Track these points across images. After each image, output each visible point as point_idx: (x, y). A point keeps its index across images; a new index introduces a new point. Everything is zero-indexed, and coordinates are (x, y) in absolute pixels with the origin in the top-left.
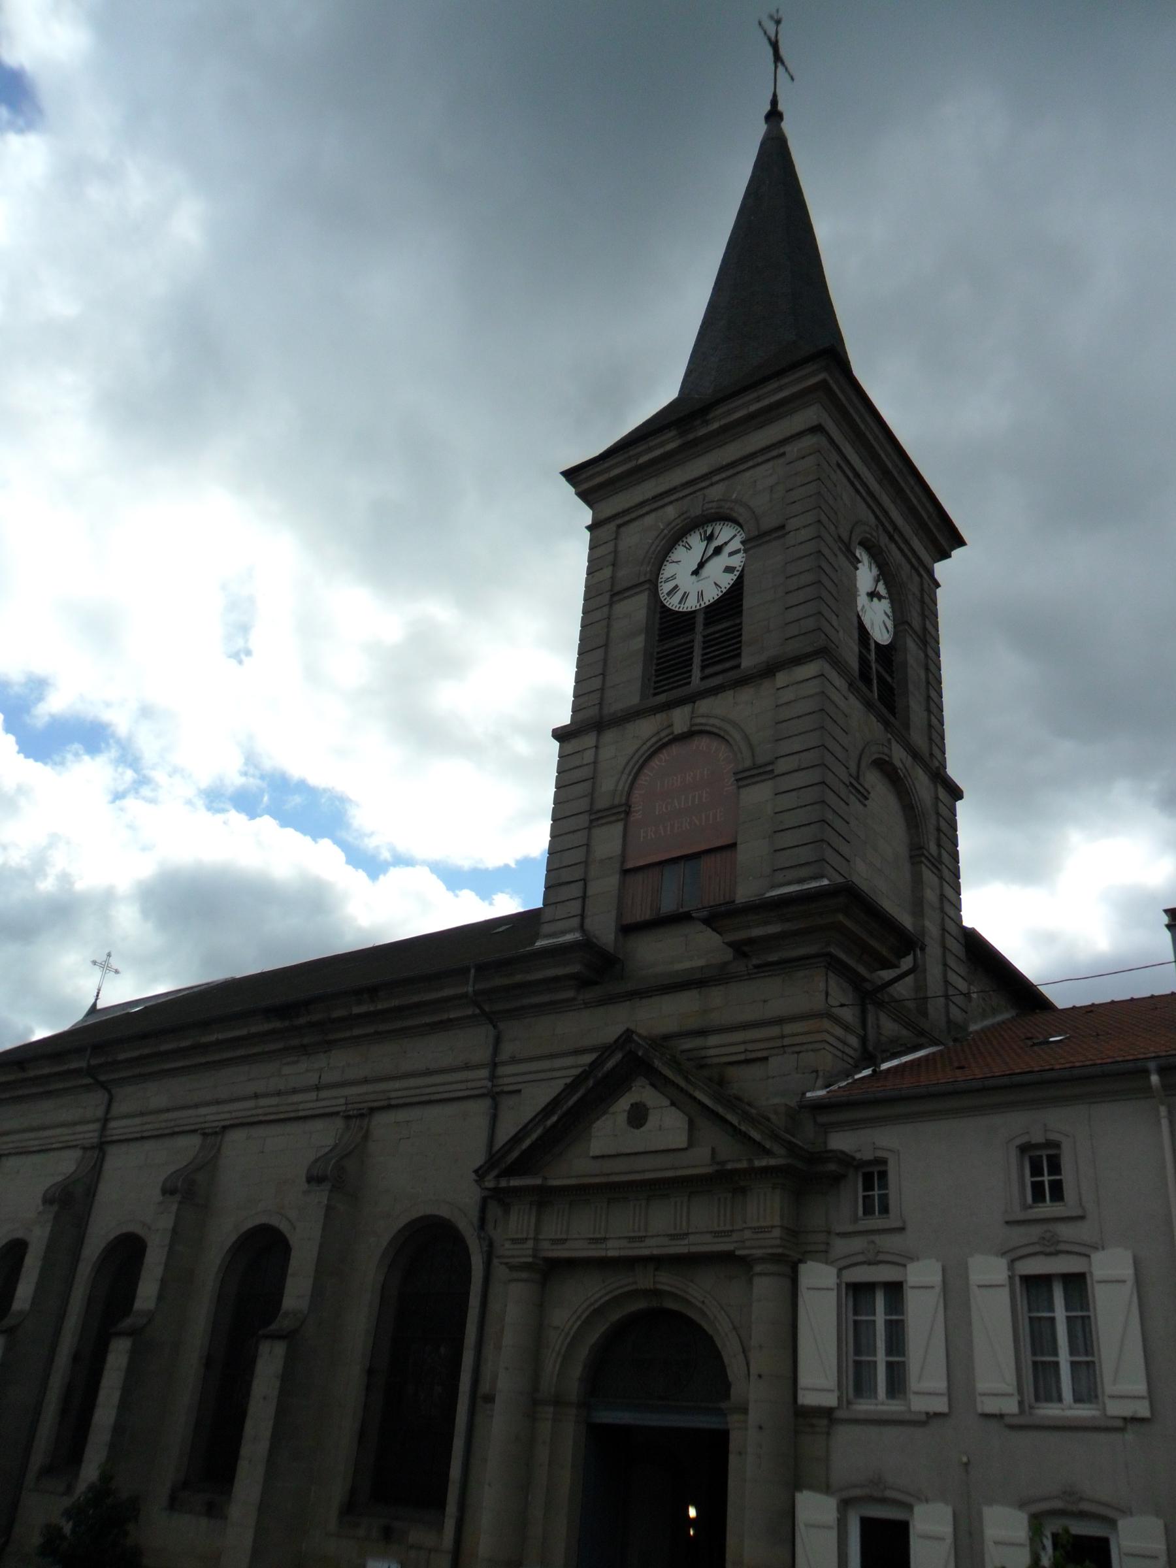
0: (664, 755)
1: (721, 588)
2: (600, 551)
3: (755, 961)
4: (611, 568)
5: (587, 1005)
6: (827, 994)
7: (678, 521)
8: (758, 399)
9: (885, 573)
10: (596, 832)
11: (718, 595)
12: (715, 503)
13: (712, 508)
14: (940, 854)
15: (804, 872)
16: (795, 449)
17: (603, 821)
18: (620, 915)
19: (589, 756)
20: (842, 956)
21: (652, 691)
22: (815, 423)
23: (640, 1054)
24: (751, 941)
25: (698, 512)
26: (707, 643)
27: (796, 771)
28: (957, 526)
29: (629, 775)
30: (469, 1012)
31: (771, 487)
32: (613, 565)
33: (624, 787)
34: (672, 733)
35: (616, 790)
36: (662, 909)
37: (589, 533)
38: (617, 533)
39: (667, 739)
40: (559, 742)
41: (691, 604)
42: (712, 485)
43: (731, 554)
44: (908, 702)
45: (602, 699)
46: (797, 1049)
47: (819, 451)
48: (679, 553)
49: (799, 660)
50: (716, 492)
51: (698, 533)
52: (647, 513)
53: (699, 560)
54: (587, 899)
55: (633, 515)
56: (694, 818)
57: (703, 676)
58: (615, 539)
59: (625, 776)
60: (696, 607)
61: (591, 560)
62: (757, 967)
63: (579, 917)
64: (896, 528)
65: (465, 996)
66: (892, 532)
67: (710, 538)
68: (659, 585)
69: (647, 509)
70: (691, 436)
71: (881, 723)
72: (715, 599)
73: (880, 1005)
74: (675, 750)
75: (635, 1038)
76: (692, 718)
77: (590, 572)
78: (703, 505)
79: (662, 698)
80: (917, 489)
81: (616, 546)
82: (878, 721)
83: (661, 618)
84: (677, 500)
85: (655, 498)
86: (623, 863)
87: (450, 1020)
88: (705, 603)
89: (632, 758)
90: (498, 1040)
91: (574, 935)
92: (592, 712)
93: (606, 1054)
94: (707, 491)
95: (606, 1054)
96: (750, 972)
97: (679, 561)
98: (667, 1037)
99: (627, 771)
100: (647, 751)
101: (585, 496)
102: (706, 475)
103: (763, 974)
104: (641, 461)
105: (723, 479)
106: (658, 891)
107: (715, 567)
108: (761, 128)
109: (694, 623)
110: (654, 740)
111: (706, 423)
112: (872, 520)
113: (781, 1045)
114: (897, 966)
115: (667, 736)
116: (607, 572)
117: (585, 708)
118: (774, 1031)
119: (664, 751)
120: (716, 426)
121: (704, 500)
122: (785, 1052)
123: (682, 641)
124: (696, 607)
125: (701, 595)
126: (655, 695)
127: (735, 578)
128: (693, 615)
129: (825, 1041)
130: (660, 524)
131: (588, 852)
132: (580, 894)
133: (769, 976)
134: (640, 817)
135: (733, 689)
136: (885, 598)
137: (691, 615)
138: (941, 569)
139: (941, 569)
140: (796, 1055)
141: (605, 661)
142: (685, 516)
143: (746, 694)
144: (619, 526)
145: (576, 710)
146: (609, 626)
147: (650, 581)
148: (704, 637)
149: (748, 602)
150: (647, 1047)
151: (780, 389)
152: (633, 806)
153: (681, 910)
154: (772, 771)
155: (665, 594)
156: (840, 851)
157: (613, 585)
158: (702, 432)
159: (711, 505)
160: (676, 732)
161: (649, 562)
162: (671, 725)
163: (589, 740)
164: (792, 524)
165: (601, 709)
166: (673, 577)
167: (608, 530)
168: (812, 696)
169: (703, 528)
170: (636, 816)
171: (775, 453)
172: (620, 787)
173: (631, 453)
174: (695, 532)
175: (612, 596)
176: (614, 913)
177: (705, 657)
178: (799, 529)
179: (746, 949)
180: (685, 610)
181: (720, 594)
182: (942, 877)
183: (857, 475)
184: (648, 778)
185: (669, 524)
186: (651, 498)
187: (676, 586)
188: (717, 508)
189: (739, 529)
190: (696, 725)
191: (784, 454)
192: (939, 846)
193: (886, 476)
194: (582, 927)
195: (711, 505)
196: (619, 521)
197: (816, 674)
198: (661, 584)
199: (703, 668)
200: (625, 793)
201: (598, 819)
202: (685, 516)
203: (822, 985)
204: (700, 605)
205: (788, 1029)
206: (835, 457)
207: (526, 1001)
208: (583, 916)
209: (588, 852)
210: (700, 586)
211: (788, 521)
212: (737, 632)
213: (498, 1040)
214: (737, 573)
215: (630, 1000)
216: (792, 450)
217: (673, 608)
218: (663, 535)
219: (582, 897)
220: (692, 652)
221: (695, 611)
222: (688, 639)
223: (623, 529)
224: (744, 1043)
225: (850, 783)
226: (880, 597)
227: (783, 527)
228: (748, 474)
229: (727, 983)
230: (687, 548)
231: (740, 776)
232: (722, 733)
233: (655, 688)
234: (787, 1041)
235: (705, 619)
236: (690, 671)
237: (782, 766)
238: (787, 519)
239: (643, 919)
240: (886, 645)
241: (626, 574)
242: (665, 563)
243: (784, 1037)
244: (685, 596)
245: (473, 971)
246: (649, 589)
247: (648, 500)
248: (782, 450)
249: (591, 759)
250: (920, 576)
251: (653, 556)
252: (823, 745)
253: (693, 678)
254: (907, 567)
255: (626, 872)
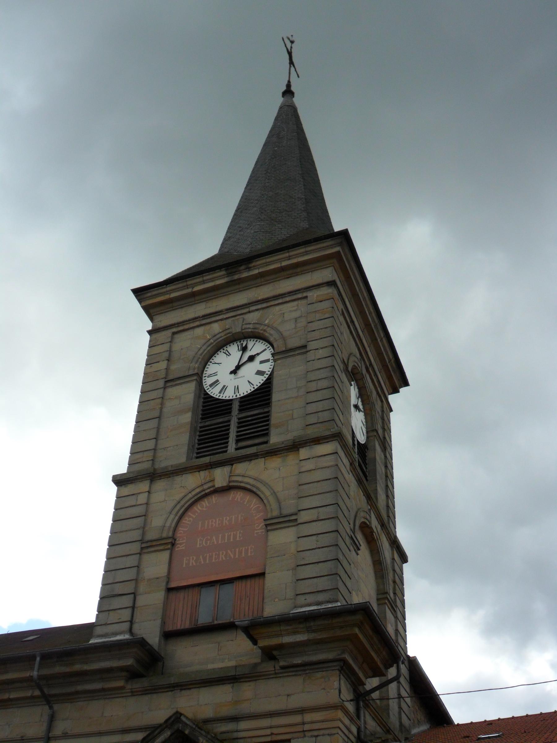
0: (205, 503)
1: (253, 385)
2: (157, 350)
3: (282, 663)
4: (166, 362)
5: (134, 693)
6: (340, 692)
7: (222, 334)
8: (289, 258)
9: (363, 394)
10: (146, 558)
11: (251, 390)
12: (251, 325)
13: (249, 328)
14: (395, 599)
15: (321, 597)
16: (315, 295)
17: (153, 549)
18: (163, 623)
19: (142, 499)
20: (351, 661)
21: (195, 455)
22: (331, 279)
23: (187, 732)
24: (281, 647)
25: (238, 330)
26: (241, 423)
27: (316, 521)
28: (405, 371)
29: (176, 515)
30: (29, 694)
31: (296, 318)
32: (168, 360)
33: (171, 524)
34: (214, 486)
35: (164, 526)
36: (199, 621)
37: (149, 336)
38: (172, 338)
39: (209, 490)
40: (117, 486)
41: (229, 395)
42: (249, 312)
43: (261, 362)
44: (377, 486)
45: (154, 456)
46: (315, 733)
47: (333, 298)
48: (220, 357)
49: (318, 441)
50: (253, 317)
51: (236, 345)
52: (198, 326)
53: (237, 364)
54: (135, 609)
55: (186, 327)
56: (229, 551)
57: (238, 447)
58: (170, 342)
59: (172, 516)
60: (233, 397)
61: (150, 355)
62: (283, 668)
63: (128, 623)
64: (371, 364)
65: (30, 679)
66: (368, 366)
67: (244, 349)
68: (204, 378)
69: (197, 323)
70: (236, 277)
71: (365, 497)
72: (249, 392)
73: (367, 706)
74: (214, 499)
75: (183, 718)
76: (230, 476)
77: (149, 363)
78: (243, 325)
79: (207, 460)
80: (384, 340)
81: (171, 347)
82: (364, 495)
83: (204, 403)
84: (221, 320)
85: (205, 316)
86: (168, 582)
87: (10, 700)
88: (240, 395)
89: (179, 502)
90: (52, 718)
91: (124, 636)
92: (146, 466)
93: (157, 732)
94: (246, 316)
95: (157, 732)
96: (276, 671)
97: (221, 363)
98: (207, 721)
99: (174, 512)
100: (191, 498)
101: (148, 310)
102: (246, 305)
103: (286, 674)
104: (197, 289)
105: (257, 310)
106: (196, 606)
107: (249, 370)
108: (280, 100)
109: (231, 408)
110: (198, 490)
111: (249, 269)
112: (358, 355)
113: (301, 730)
114: (384, 675)
115: (209, 488)
116: (163, 365)
117: (140, 462)
118: (297, 719)
119: (206, 500)
120: (256, 272)
121: (243, 322)
122: (305, 736)
123: (221, 420)
124: (233, 397)
125: (237, 389)
126: (197, 458)
127: (265, 379)
128: (230, 402)
129: (339, 728)
130: (208, 335)
131: (138, 573)
132: (131, 604)
133: (295, 675)
134: (184, 548)
135: (264, 457)
136: (362, 411)
137: (229, 403)
138: (393, 399)
139: (393, 399)
140: (314, 738)
141: (158, 429)
142: (228, 331)
143: (275, 462)
144: (174, 333)
145: (131, 463)
146: (162, 404)
147: (197, 374)
148: (239, 419)
149: (276, 397)
150: (194, 726)
151: (307, 253)
152: (177, 539)
153: (216, 622)
154: (296, 520)
155: (208, 385)
156: (346, 584)
157: (167, 374)
158: (245, 275)
159: (248, 326)
160: (216, 486)
161: (197, 361)
162: (213, 480)
163: (144, 486)
164: (312, 345)
165: (153, 464)
166: (215, 374)
167: (165, 336)
168: (331, 466)
169: (240, 342)
170: (180, 547)
171: (300, 296)
172: (168, 524)
173: (189, 283)
174: (233, 344)
175: (166, 382)
176: (159, 622)
177: (239, 434)
178: (317, 349)
179: (275, 653)
180: (224, 398)
181: (253, 390)
182: (397, 617)
183: (352, 322)
184: (191, 519)
185: (215, 336)
186: (201, 316)
187: (217, 381)
188: (253, 328)
189: (269, 345)
190: (234, 481)
191: (306, 297)
192: (395, 594)
193: (367, 325)
194: (131, 631)
195: (248, 326)
196: (175, 330)
197: (334, 452)
198: (205, 378)
199: (237, 441)
200: (172, 529)
201: (147, 547)
202: (228, 331)
203: (336, 684)
204: (236, 396)
205: (308, 717)
206: (341, 306)
207: (80, 688)
208: (131, 622)
209: (138, 573)
210: (236, 382)
211: (309, 343)
212: (266, 418)
213: (52, 718)
214: (267, 376)
215: (172, 691)
216: (313, 295)
217: (214, 396)
218: (209, 343)
219: (132, 607)
220: (229, 429)
221: (231, 400)
222: (226, 419)
223: (176, 336)
224: (271, 727)
225: (351, 536)
226: (360, 410)
227: (305, 347)
228: (277, 308)
229: (256, 680)
230: (227, 355)
231: (268, 522)
232: (254, 489)
233: (197, 453)
234: (307, 727)
235: (240, 406)
236: (227, 443)
237: (304, 517)
238: (308, 342)
239: (182, 628)
240: (361, 444)
241: (178, 368)
242: (209, 363)
243: (305, 724)
244: (224, 388)
245: (38, 659)
246: (196, 379)
247: (199, 317)
248: (305, 294)
249: (145, 501)
250: (382, 401)
251: (201, 357)
252: (337, 504)
253: (229, 448)
254: (374, 393)
255: (169, 590)
